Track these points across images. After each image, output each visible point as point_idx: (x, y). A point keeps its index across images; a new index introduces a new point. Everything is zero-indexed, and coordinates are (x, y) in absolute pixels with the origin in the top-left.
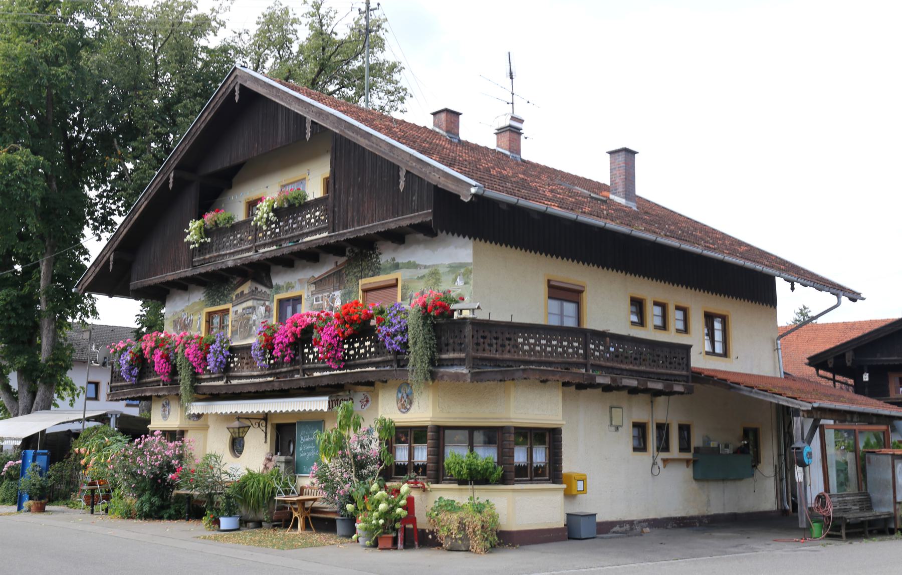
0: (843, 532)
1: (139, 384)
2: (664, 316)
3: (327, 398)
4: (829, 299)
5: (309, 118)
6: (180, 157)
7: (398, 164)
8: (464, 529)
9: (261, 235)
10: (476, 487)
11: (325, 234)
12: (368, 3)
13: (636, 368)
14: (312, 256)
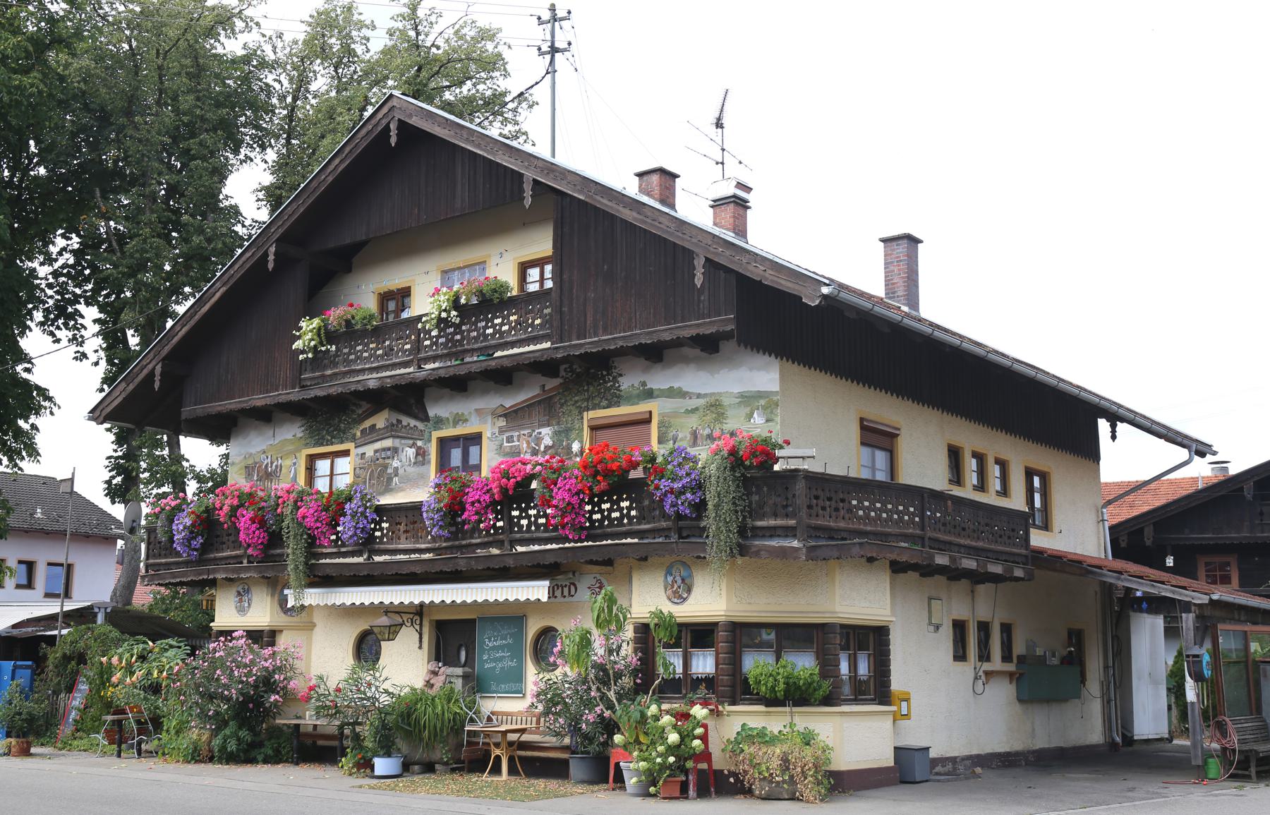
0: (1253, 770)
1: (200, 562)
2: (982, 472)
3: (547, 583)
4: (1183, 454)
5: (529, 174)
6: (288, 224)
7: (687, 245)
8: (788, 769)
9: (427, 343)
10: (795, 709)
11: (547, 345)
12: (553, 9)
13: (974, 544)
14: (502, 377)
